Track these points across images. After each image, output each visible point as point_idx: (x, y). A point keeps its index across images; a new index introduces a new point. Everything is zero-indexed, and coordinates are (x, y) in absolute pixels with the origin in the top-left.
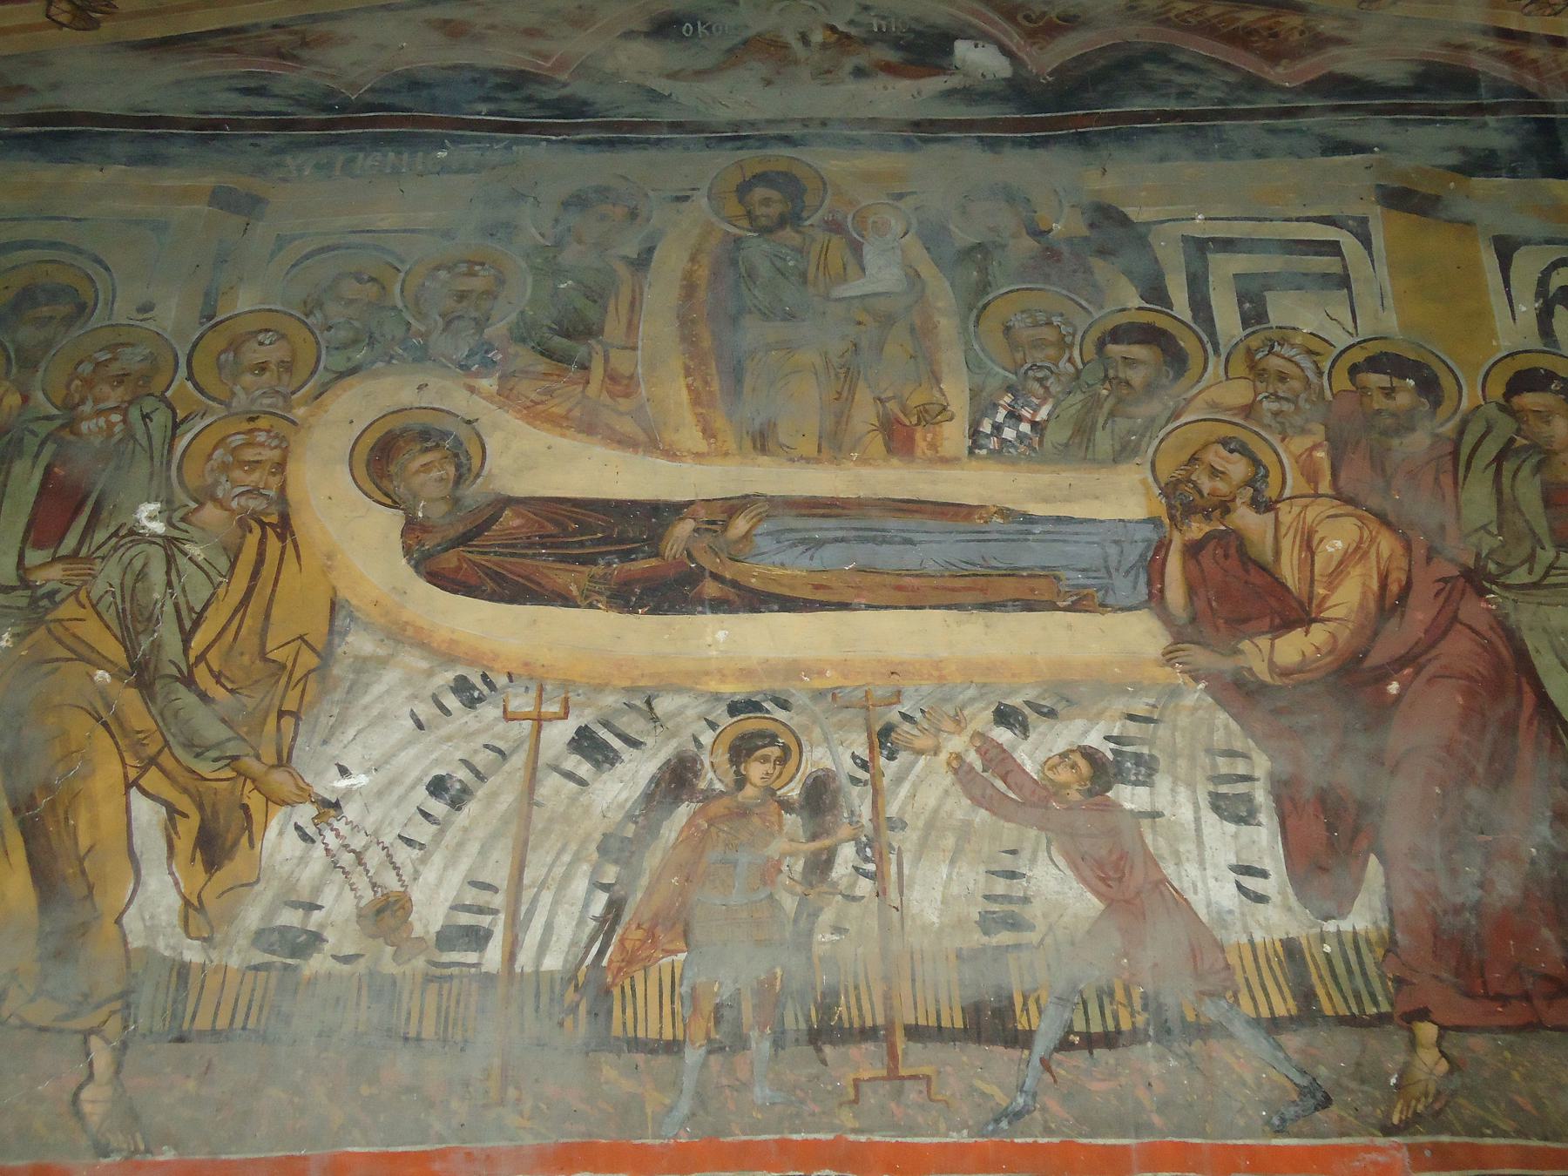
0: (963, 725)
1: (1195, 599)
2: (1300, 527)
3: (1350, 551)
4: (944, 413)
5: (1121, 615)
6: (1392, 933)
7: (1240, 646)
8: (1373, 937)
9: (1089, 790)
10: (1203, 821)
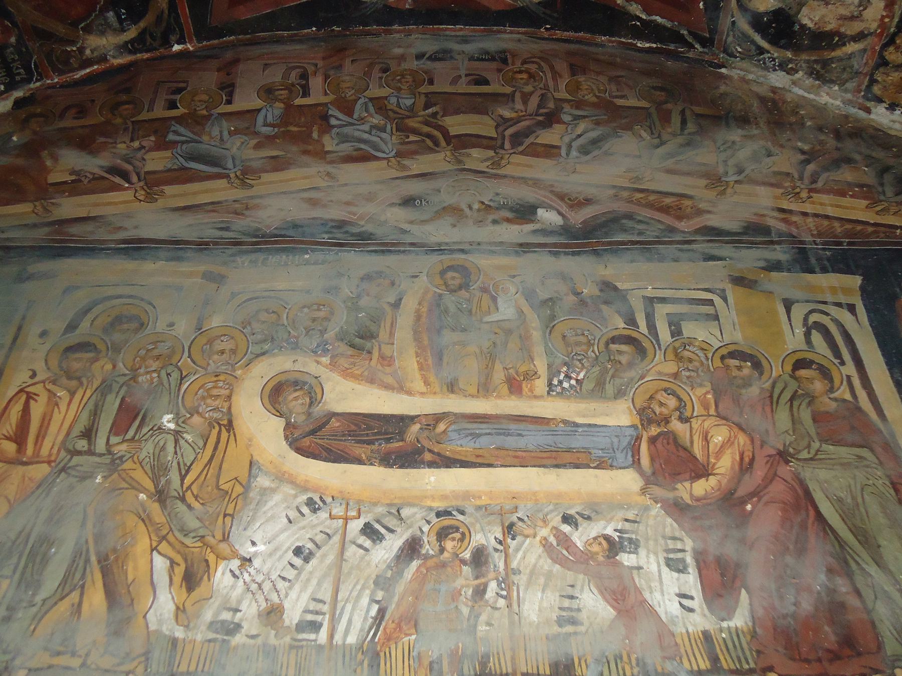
1: (77, 479)
6: (754, 627)
8: (745, 629)
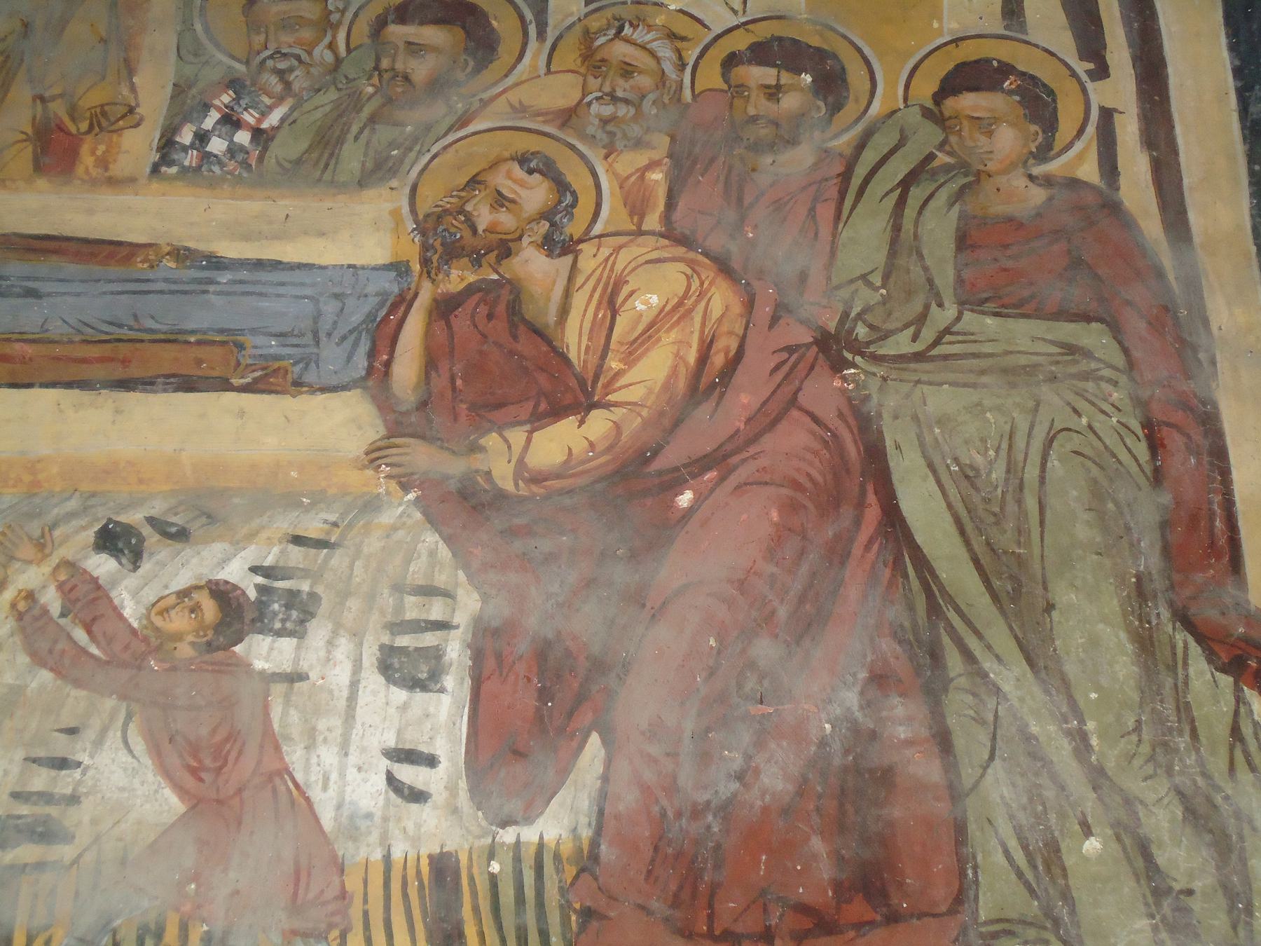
0: (47, 551)
1: (433, 374)
2: (605, 276)
3: (668, 308)
4: (129, 117)
5: (321, 398)
6: (594, 844)
7: (482, 441)
8: (567, 849)
9: (209, 644)
10: (361, 686)
